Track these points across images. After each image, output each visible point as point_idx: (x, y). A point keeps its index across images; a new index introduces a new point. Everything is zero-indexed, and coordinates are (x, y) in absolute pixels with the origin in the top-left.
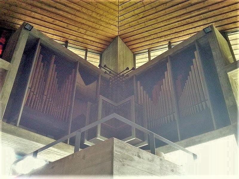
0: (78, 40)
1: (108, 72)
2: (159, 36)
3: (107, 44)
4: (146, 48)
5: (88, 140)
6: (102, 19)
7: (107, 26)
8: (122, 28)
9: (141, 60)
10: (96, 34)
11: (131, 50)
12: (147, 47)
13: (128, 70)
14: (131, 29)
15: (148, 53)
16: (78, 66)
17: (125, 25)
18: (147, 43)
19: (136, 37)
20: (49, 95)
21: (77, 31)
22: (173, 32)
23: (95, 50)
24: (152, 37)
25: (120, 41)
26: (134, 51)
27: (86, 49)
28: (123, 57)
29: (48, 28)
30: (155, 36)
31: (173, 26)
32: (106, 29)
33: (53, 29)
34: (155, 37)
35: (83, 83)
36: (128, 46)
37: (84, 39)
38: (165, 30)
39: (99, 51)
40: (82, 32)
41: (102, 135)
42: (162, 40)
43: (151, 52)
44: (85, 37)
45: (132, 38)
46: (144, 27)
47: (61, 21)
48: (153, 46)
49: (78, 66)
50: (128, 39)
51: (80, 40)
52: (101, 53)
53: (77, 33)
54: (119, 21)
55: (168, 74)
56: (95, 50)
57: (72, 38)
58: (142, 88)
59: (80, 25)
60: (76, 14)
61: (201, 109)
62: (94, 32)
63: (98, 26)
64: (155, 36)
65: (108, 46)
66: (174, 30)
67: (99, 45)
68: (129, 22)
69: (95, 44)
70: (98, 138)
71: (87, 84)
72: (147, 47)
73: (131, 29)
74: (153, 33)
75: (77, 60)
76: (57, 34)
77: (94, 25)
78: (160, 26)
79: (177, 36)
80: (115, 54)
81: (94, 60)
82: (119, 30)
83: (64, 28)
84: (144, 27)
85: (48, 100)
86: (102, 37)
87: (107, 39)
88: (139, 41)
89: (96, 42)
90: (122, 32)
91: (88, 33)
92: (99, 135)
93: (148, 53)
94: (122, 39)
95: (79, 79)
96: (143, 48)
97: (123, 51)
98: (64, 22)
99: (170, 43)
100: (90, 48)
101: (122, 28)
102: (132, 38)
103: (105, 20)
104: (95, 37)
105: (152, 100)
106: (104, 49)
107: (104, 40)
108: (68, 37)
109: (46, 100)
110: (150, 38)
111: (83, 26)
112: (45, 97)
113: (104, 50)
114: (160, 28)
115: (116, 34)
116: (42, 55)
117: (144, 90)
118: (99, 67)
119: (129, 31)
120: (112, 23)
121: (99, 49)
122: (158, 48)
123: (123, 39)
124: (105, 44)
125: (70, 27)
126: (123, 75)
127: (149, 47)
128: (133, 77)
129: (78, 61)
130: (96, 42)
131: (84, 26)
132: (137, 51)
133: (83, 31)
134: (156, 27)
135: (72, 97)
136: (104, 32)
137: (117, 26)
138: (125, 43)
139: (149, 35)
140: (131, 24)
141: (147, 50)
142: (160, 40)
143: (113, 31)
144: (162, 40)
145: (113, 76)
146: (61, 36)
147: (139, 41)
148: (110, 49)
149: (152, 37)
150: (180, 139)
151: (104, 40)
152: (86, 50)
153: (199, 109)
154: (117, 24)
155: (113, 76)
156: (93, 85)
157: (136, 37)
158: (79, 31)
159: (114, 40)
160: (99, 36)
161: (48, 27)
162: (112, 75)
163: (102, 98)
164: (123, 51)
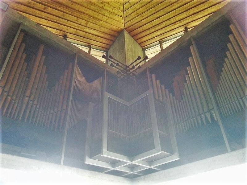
0: (78, 34)
1: (115, 65)
2: (173, 22)
3: (112, 38)
4: (157, 40)
5: (91, 157)
6: (105, 7)
7: (111, 16)
8: (128, 19)
9: (152, 53)
10: (99, 27)
11: (139, 44)
12: (158, 38)
13: (140, 60)
14: (139, 18)
15: (159, 45)
16: (76, 59)
17: (132, 14)
18: (159, 33)
19: (145, 27)
20: (33, 96)
21: (76, 22)
22: (190, 14)
23: (99, 46)
24: (164, 24)
25: (126, 35)
26: (143, 45)
27: (89, 46)
28: (132, 51)
29: (39, 17)
30: (168, 23)
31: (191, 5)
32: (110, 21)
33: (45, 19)
34: (167, 24)
35: (84, 80)
36: (136, 40)
37: (86, 32)
38: (181, 12)
39: (103, 47)
40: (82, 24)
41: (110, 149)
42: (177, 26)
43: (163, 43)
44: (87, 30)
45: (140, 30)
46: (154, 13)
47: (55, 9)
48: (164, 36)
49: (76, 59)
50: (136, 32)
51: (82, 33)
52: (106, 49)
53: (76, 25)
54: (125, 10)
55: (194, 58)
56: (99, 46)
57: (71, 32)
58: (158, 82)
59: (79, 14)
60: (84, 33)
61: (200, 124)
62: (97, 23)
63: (100, 17)
64: (168, 23)
65: (113, 41)
66: (192, 12)
67: (104, 41)
68: (136, 9)
69: (98, 39)
70: (103, 155)
71: (89, 80)
72: (158, 38)
73: (139, 18)
74: (165, 20)
75: (75, 52)
76: (52, 26)
77: (96, 15)
78: (174, 8)
79: (194, 19)
80: (123, 48)
81: (98, 55)
82: (125, 22)
83: (60, 17)
84: (154, 13)
85: (35, 106)
86: (106, 30)
87: (113, 33)
88: (148, 32)
89: (100, 37)
90: (129, 24)
91: (90, 25)
92: (105, 150)
93: (159, 45)
94: (129, 33)
95: (78, 76)
96: (153, 40)
97: (131, 46)
98: (58, 10)
99: (186, 29)
100: (93, 44)
101: (128, 19)
102: (140, 30)
103: (107, 8)
104: (98, 31)
105: (173, 95)
106: (110, 46)
107: (109, 35)
108: (65, 30)
109: (32, 106)
110: (162, 26)
111: (83, 16)
112: (27, 99)
113: (110, 46)
114: (174, 11)
115: (122, 27)
116: (46, 66)
117: (161, 84)
118: (104, 60)
119: (137, 21)
120: (116, 12)
121: (103, 45)
122: (173, 37)
123: (130, 32)
124: (110, 39)
125: (67, 16)
126: (134, 67)
127: (160, 38)
128: (146, 70)
129: (76, 53)
130: (100, 37)
131: (84, 16)
132: (146, 45)
133: (83, 23)
134: (168, 11)
135: (68, 98)
136: (108, 25)
137: (123, 16)
138: (133, 36)
139: (161, 22)
140: (138, 11)
141: (158, 42)
142: (173, 27)
143: (119, 23)
144: (177, 26)
145: (122, 69)
146: (58, 28)
147: (148, 32)
148: (117, 45)
149: (164, 24)
150: (62, 163)
151: (109, 35)
152: (90, 47)
153: (198, 124)
154: (122, 14)
155: (122, 69)
156: (97, 83)
157: (145, 27)
158: (79, 23)
159: (120, 33)
160: (102, 29)
161: (39, 16)
162: (120, 68)
163: (107, 95)
164: (131, 46)
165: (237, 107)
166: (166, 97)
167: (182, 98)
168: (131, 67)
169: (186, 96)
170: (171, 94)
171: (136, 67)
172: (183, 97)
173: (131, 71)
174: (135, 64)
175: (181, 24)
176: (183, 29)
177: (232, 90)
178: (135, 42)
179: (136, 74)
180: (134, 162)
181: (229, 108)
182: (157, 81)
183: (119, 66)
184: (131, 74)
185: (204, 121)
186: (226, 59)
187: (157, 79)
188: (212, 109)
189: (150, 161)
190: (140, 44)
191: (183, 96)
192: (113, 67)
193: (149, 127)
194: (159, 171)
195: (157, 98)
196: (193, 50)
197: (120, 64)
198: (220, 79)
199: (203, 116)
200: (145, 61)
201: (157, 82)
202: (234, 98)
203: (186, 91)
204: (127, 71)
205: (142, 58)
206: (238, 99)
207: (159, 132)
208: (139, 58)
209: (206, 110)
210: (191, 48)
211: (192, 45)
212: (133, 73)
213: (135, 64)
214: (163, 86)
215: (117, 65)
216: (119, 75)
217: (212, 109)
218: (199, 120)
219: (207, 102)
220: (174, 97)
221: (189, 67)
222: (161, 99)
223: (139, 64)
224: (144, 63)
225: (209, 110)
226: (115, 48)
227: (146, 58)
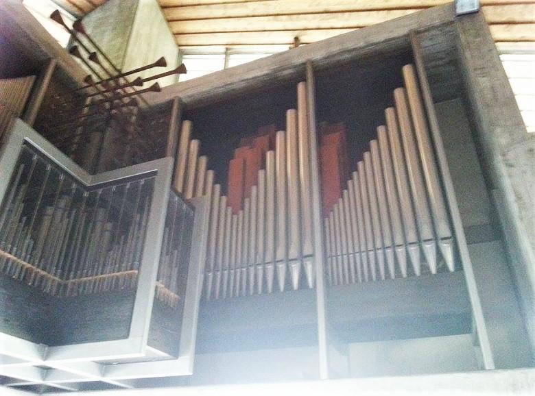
1: (85, 55)
26: (183, 40)
55: (300, 119)
58: (195, 144)
105: (224, 192)
117: (201, 153)
126: (139, 82)
128: (170, 104)
141: (223, 49)
165: (369, 271)
166: (204, 193)
167: (243, 208)
168: (132, 78)
169: (247, 215)
170: (218, 187)
171: (146, 85)
172: (247, 205)
173: (130, 90)
174: (146, 74)
175: (290, 25)
176: (291, 40)
177: (232, 282)
178: (165, 24)
179: (142, 104)
180: (48, 363)
181: (349, 270)
182: (193, 141)
183: (97, 62)
184: (126, 100)
185: (366, 277)
186: (373, 143)
187: (193, 136)
188: (311, 256)
189: (106, 366)
190: (177, 34)
191: (247, 200)
192: (78, 60)
193: (132, 269)
194: (125, 388)
195: (180, 190)
196: (304, 94)
197: (100, 58)
198: (347, 188)
199: (282, 267)
200: (177, 78)
201: (192, 146)
202: (366, 244)
203: (238, 218)
204: (118, 86)
205: (171, 66)
206: (375, 249)
207: (156, 287)
208: (161, 63)
209: (294, 253)
210: (301, 87)
211: (305, 80)
212: (133, 97)
213: (146, 74)
214: (204, 160)
215: (93, 57)
216: (90, 90)
217: (311, 256)
218: (352, 261)
219: (301, 235)
220: (224, 199)
221: (272, 152)
222: (189, 196)
223: (159, 80)
224: (171, 84)
225: (302, 257)
226: (106, 18)
227: (181, 69)
